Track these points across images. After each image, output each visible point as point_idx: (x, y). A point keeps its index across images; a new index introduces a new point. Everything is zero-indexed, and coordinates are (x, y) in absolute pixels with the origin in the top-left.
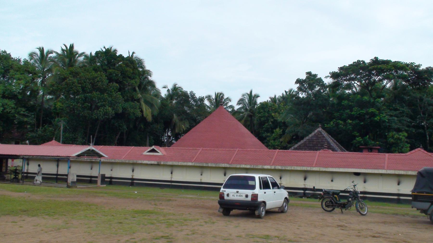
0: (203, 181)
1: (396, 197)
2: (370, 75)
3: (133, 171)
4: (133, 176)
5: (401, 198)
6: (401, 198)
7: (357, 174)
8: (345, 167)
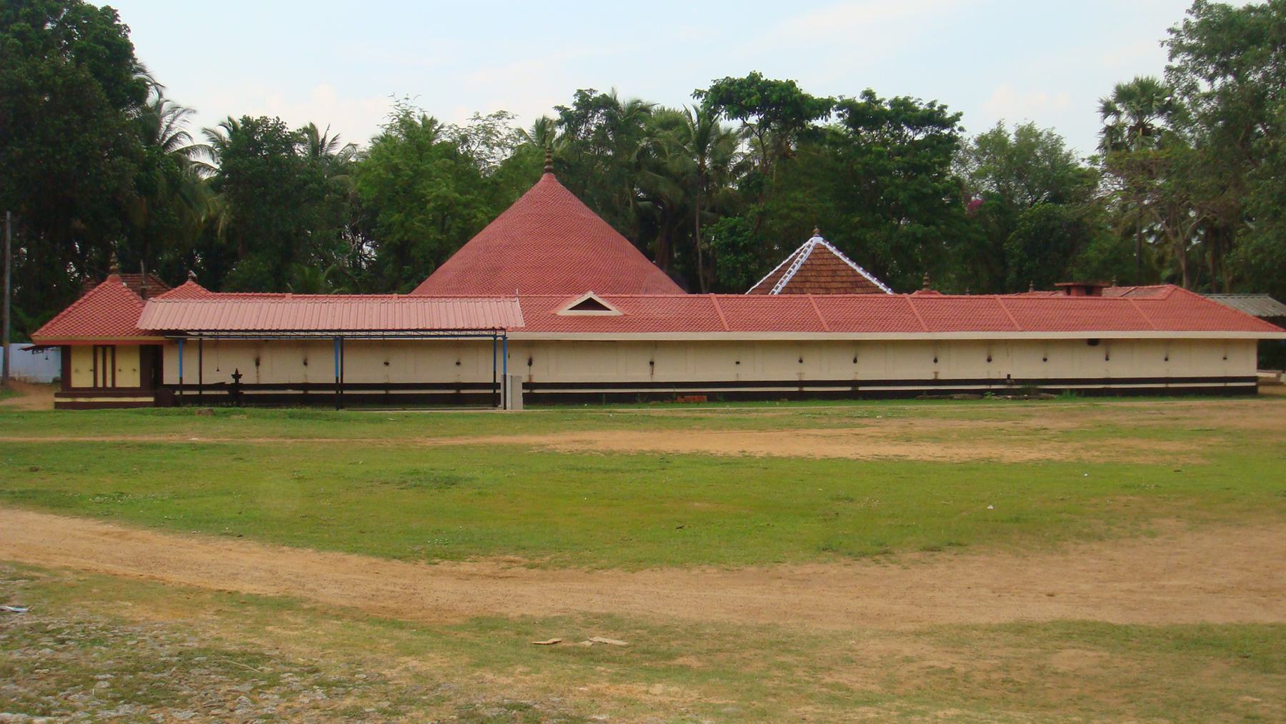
0: (941, 377)
1: (796, 389)
2: (56, 74)
3: (530, 363)
4: (530, 377)
5: (806, 389)
6: (806, 389)
7: (1093, 342)
8: (745, 328)
